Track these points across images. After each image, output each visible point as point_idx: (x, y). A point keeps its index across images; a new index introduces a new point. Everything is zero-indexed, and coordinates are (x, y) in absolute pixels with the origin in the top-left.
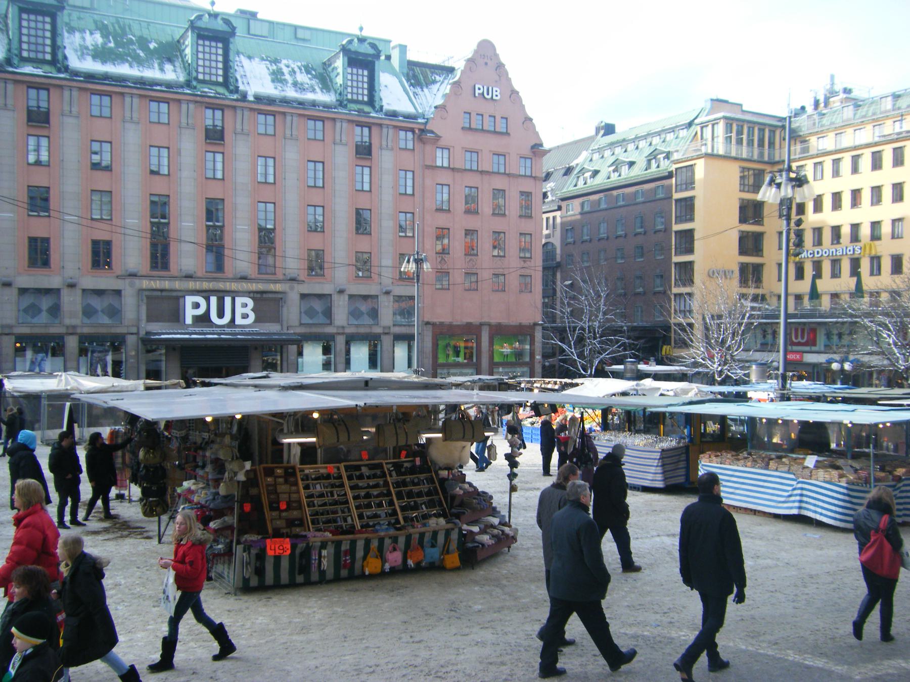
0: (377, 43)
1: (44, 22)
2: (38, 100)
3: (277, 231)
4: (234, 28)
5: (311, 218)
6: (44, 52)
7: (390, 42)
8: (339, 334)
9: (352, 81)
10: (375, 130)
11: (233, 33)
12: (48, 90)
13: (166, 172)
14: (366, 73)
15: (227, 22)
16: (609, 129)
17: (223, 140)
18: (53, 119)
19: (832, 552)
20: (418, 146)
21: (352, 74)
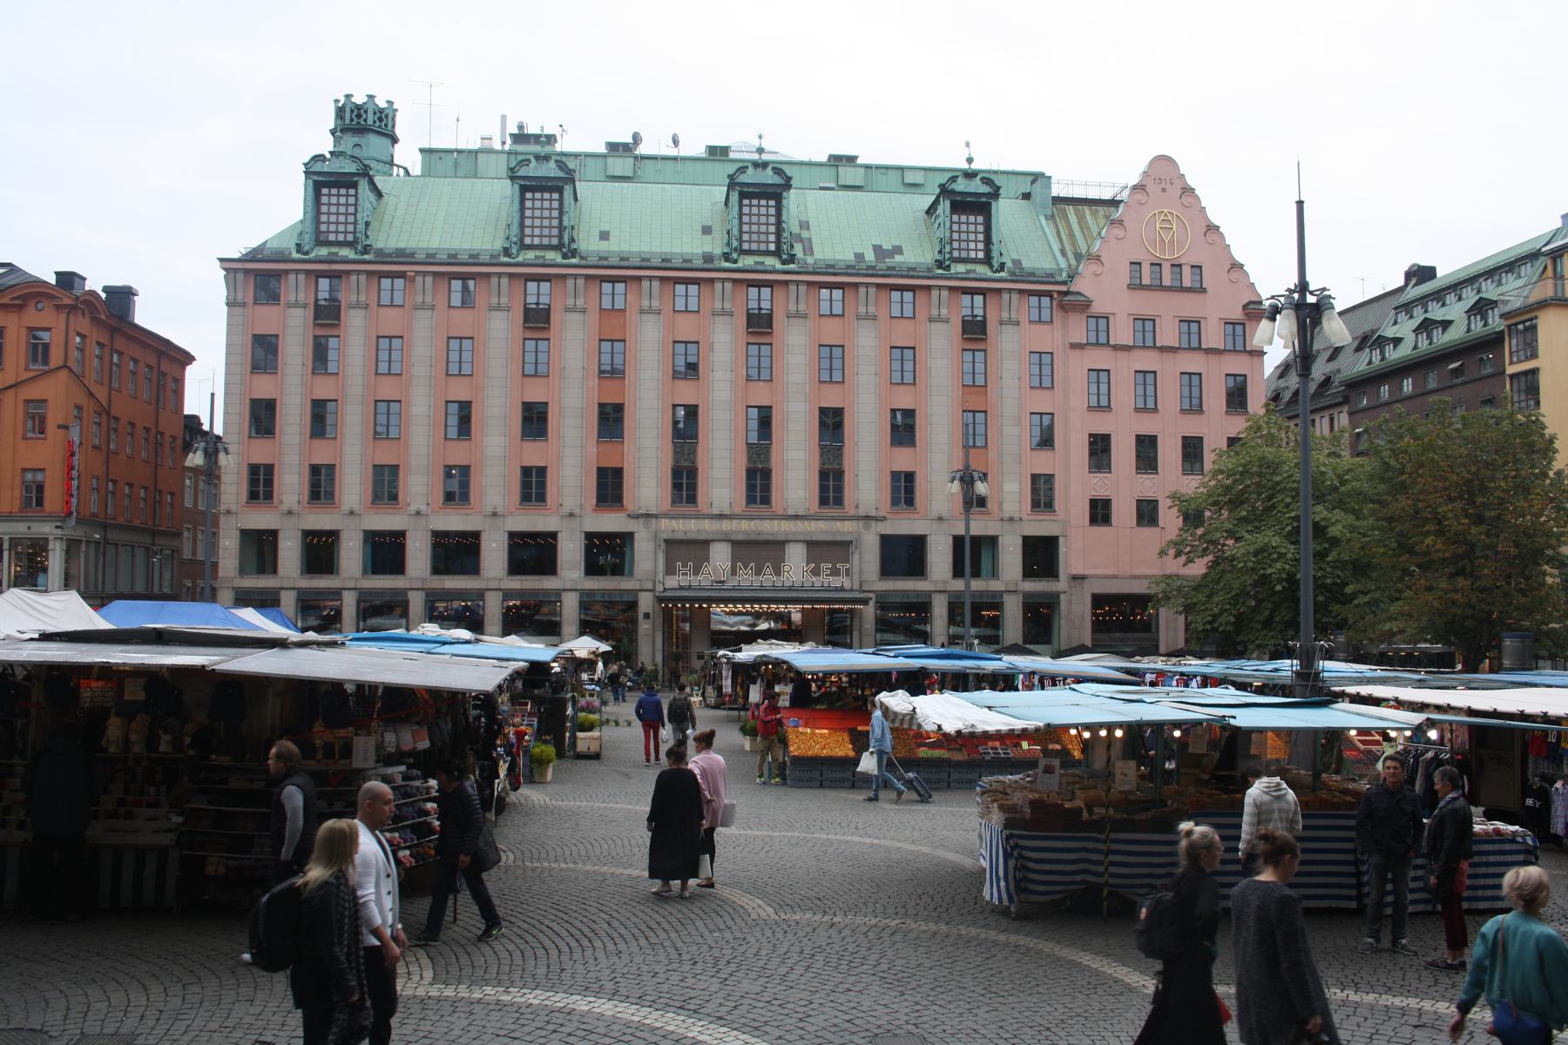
0: (992, 177)
4: (789, 179)
6: (767, 242)
14: (980, 219)
17: (548, 322)
18: (555, 317)
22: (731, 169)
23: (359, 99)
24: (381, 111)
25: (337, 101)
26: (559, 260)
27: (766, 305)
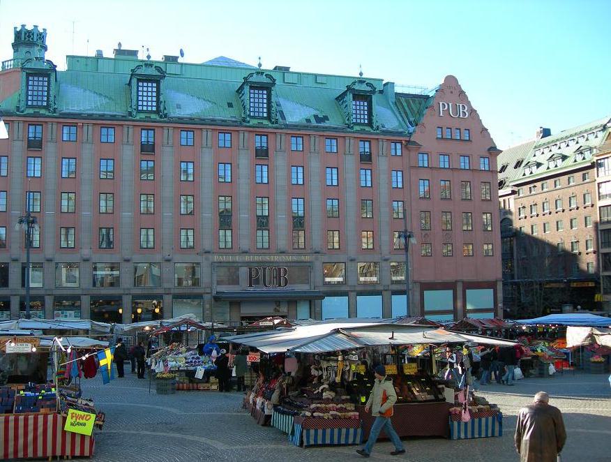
1: (263, 94)
2: (35, 133)
3: (306, 218)
5: (329, 207)
6: (42, 101)
7: (382, 80)
8: (352, 291)
9: (356, 110)
10: (373, 142)
11: (274, 84)
12: (154, 130)
13: (230, 181)
14: (366, 104)
15: (158, 69)
16: (546, 133)
17: (41, 148)
19: (306, 332)
20: (406, 152)
21: (356, 105)
22: (133, 65)
23: (29, 27)
24: (41, 34)
25: (15, 28)
26: (158, 119)
27: (151, 140)
